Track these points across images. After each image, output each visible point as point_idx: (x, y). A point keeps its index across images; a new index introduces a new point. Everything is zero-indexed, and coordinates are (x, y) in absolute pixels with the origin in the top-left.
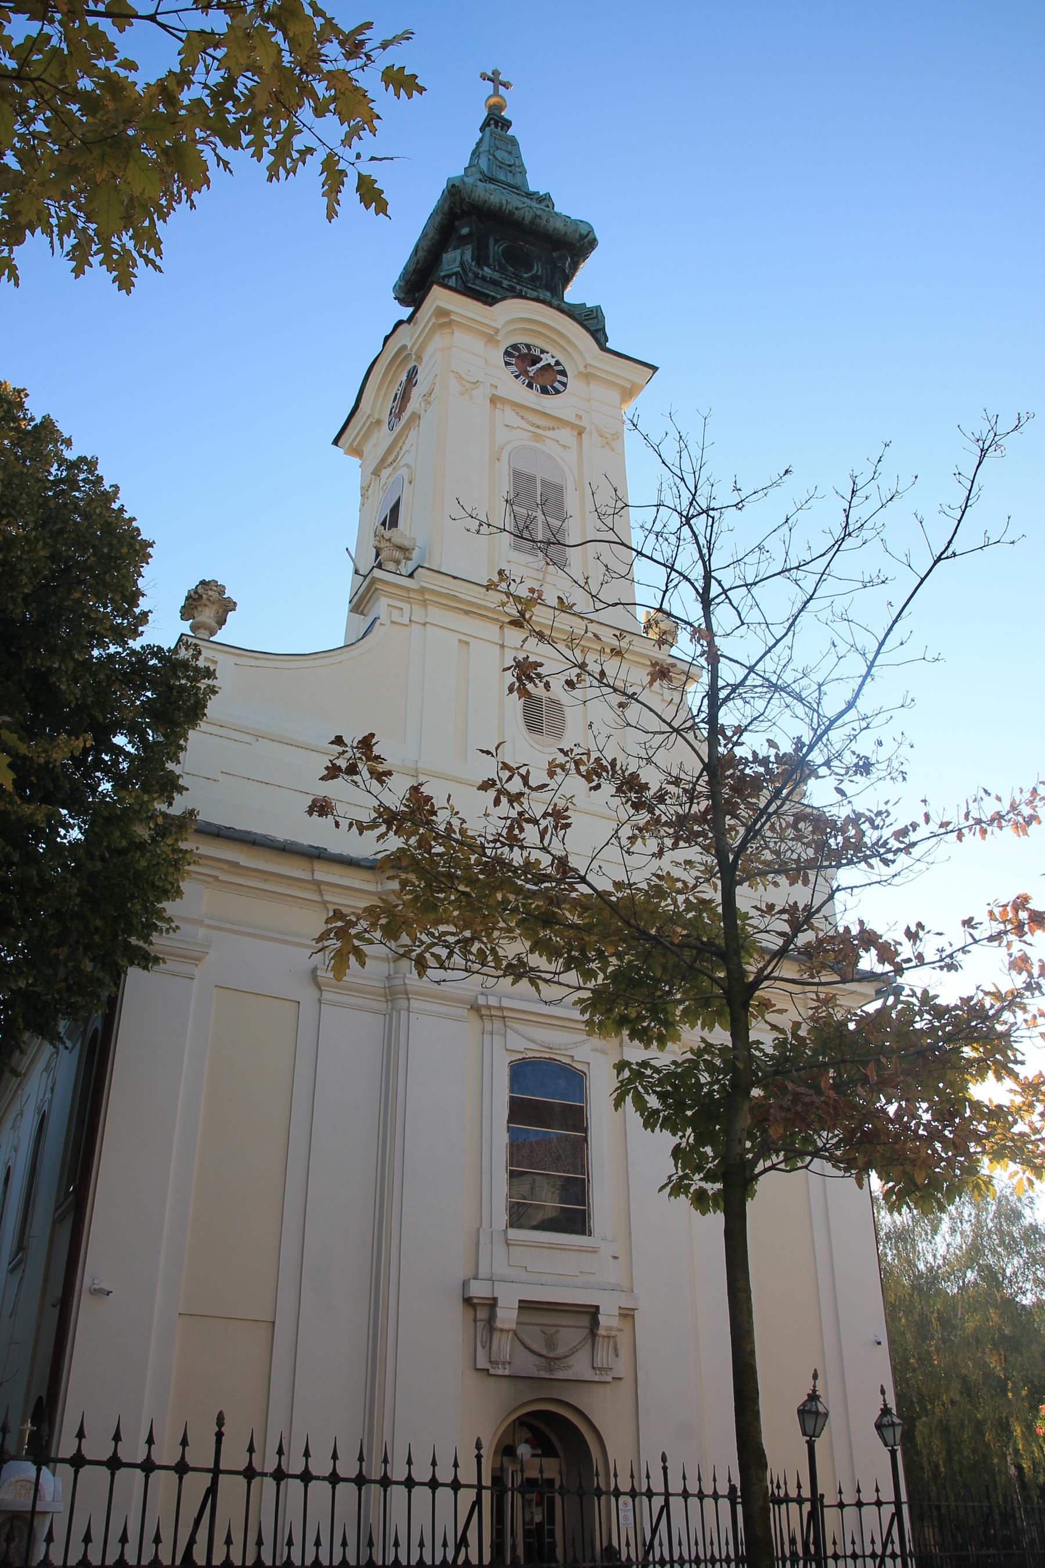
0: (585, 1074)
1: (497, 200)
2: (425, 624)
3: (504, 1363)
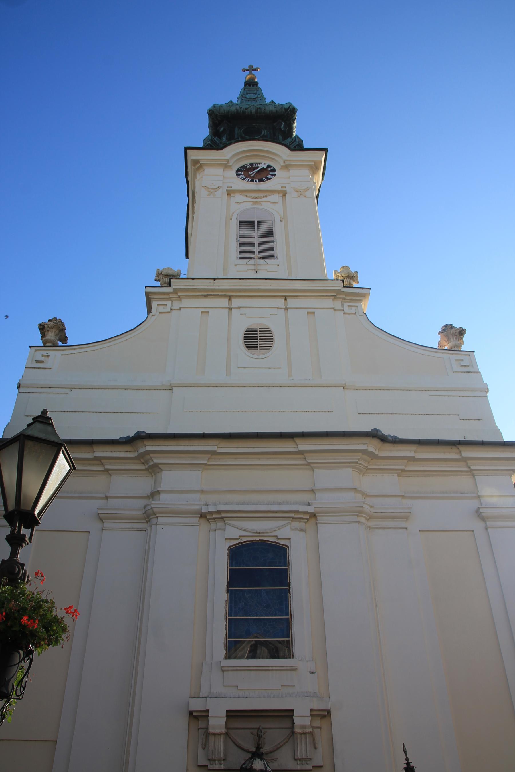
0: (288, 547)
1: (234, 108)
3: (219, 760)
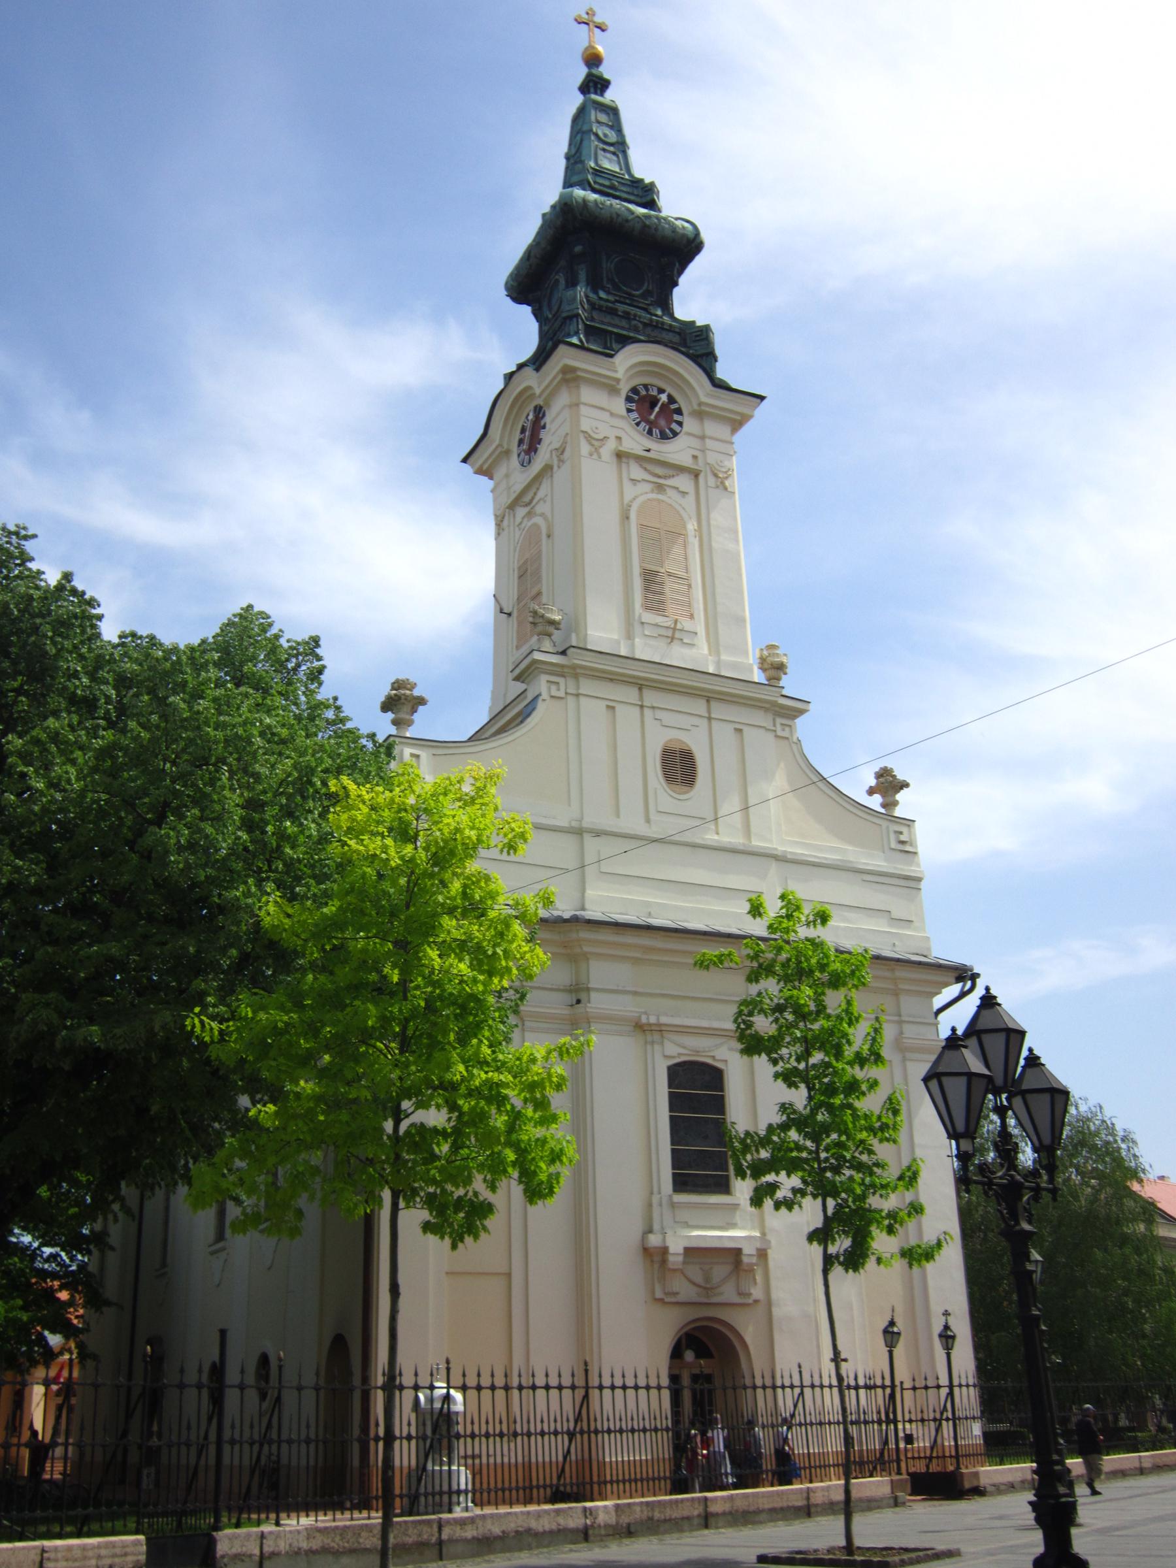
2: (577, 695)
